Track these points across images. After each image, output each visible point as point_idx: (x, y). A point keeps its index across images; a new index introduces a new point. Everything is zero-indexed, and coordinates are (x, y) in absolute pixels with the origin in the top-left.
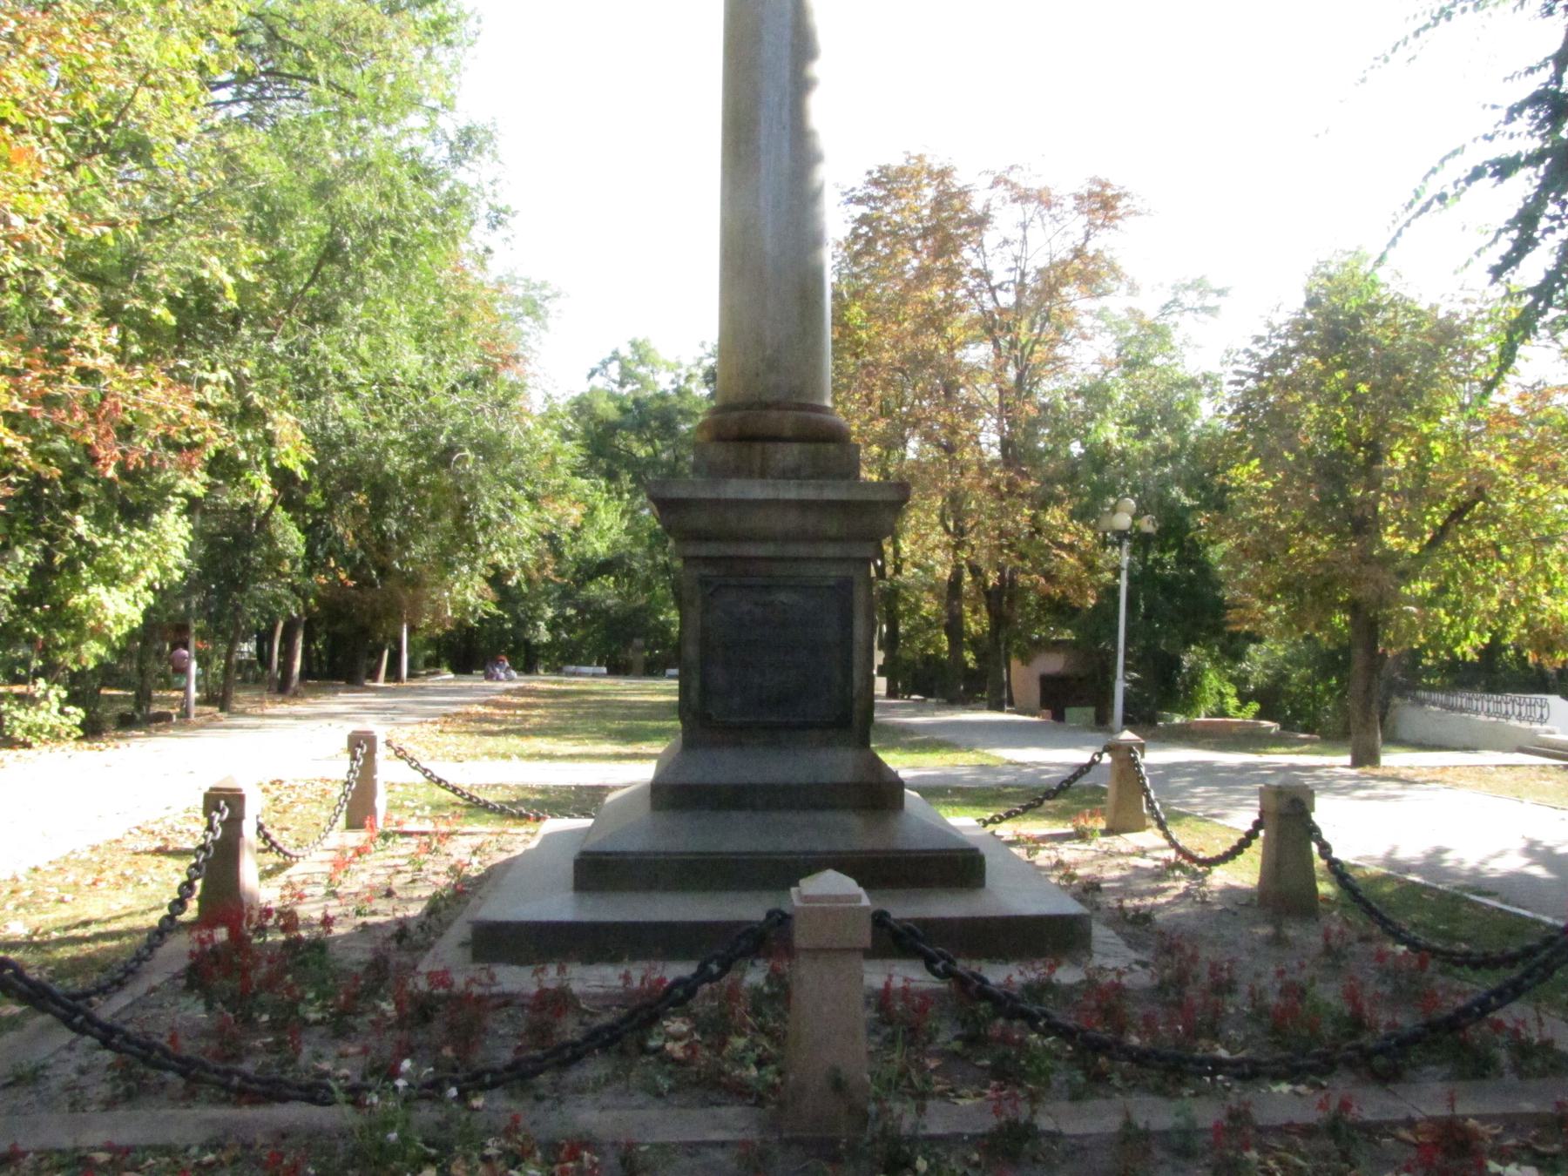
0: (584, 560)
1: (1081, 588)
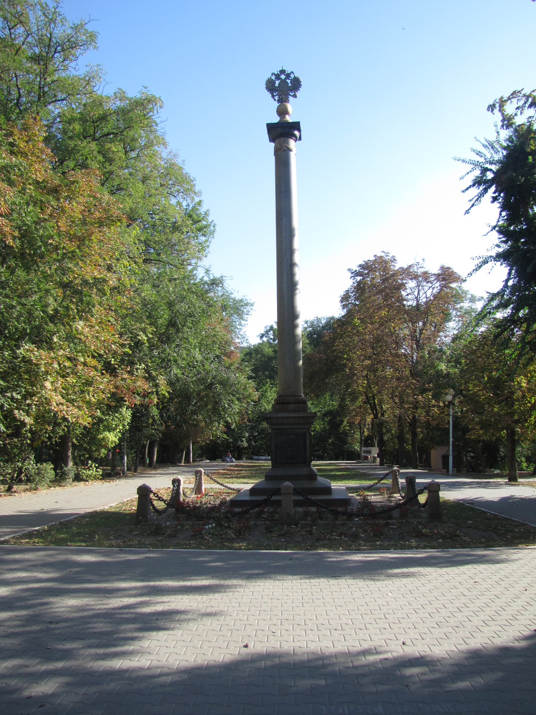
0: (261, 413)
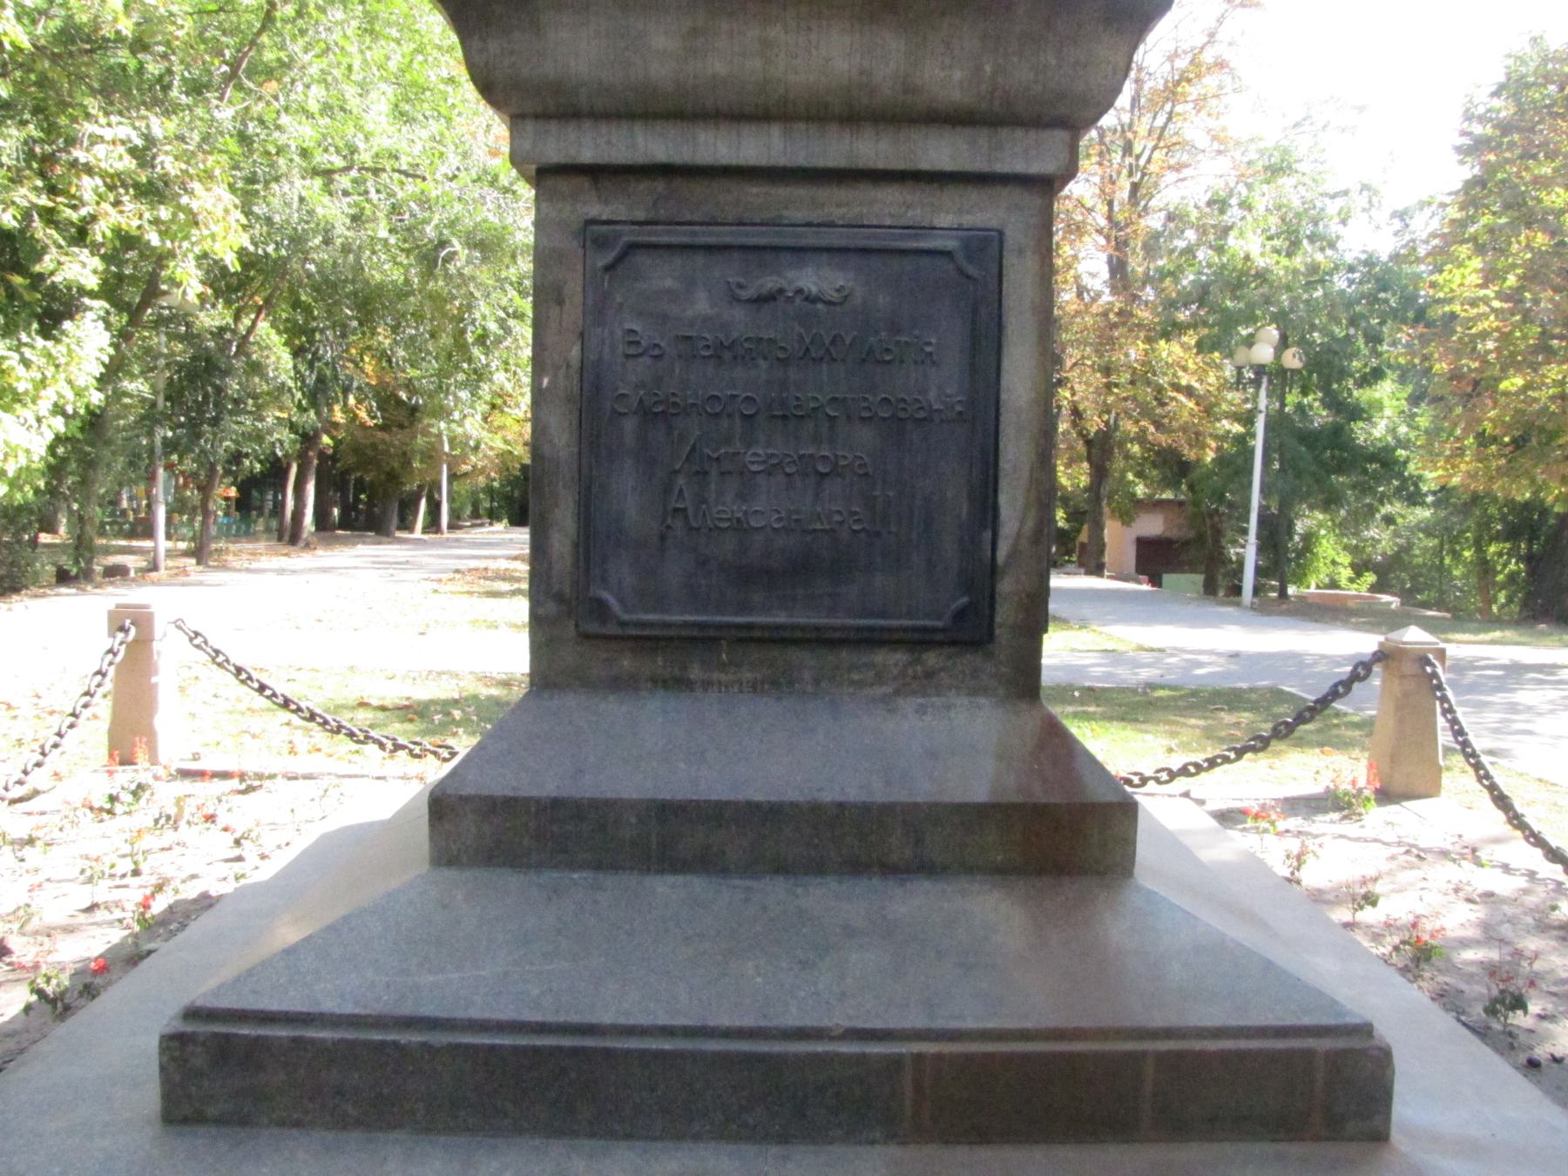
1: (1198, 441)
